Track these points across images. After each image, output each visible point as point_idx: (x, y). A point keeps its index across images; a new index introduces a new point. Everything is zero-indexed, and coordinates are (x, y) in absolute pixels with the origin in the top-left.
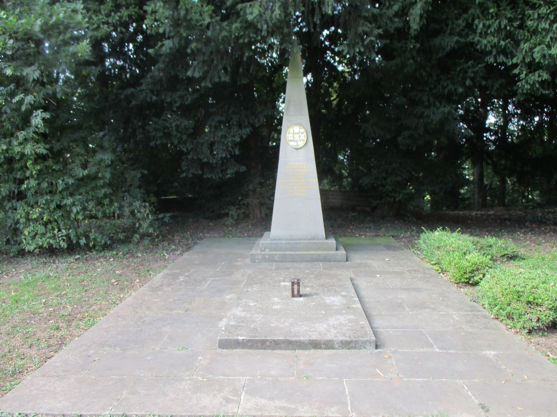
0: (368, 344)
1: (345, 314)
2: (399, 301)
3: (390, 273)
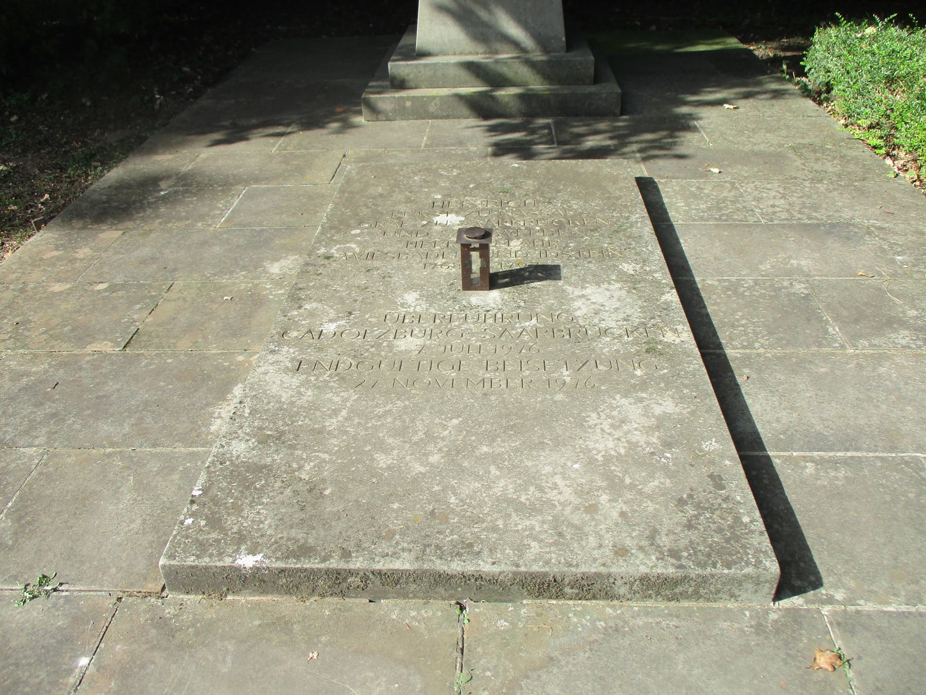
0: (750, 586)
1: (643, 385)
2: (800, 288)
3: (745, 158)
